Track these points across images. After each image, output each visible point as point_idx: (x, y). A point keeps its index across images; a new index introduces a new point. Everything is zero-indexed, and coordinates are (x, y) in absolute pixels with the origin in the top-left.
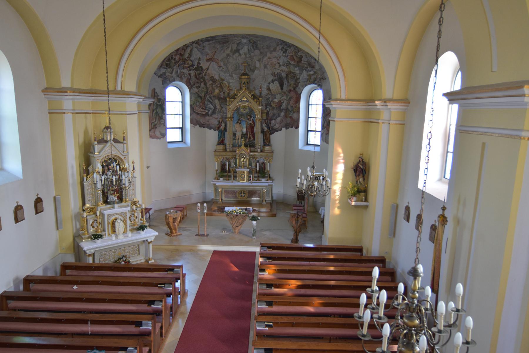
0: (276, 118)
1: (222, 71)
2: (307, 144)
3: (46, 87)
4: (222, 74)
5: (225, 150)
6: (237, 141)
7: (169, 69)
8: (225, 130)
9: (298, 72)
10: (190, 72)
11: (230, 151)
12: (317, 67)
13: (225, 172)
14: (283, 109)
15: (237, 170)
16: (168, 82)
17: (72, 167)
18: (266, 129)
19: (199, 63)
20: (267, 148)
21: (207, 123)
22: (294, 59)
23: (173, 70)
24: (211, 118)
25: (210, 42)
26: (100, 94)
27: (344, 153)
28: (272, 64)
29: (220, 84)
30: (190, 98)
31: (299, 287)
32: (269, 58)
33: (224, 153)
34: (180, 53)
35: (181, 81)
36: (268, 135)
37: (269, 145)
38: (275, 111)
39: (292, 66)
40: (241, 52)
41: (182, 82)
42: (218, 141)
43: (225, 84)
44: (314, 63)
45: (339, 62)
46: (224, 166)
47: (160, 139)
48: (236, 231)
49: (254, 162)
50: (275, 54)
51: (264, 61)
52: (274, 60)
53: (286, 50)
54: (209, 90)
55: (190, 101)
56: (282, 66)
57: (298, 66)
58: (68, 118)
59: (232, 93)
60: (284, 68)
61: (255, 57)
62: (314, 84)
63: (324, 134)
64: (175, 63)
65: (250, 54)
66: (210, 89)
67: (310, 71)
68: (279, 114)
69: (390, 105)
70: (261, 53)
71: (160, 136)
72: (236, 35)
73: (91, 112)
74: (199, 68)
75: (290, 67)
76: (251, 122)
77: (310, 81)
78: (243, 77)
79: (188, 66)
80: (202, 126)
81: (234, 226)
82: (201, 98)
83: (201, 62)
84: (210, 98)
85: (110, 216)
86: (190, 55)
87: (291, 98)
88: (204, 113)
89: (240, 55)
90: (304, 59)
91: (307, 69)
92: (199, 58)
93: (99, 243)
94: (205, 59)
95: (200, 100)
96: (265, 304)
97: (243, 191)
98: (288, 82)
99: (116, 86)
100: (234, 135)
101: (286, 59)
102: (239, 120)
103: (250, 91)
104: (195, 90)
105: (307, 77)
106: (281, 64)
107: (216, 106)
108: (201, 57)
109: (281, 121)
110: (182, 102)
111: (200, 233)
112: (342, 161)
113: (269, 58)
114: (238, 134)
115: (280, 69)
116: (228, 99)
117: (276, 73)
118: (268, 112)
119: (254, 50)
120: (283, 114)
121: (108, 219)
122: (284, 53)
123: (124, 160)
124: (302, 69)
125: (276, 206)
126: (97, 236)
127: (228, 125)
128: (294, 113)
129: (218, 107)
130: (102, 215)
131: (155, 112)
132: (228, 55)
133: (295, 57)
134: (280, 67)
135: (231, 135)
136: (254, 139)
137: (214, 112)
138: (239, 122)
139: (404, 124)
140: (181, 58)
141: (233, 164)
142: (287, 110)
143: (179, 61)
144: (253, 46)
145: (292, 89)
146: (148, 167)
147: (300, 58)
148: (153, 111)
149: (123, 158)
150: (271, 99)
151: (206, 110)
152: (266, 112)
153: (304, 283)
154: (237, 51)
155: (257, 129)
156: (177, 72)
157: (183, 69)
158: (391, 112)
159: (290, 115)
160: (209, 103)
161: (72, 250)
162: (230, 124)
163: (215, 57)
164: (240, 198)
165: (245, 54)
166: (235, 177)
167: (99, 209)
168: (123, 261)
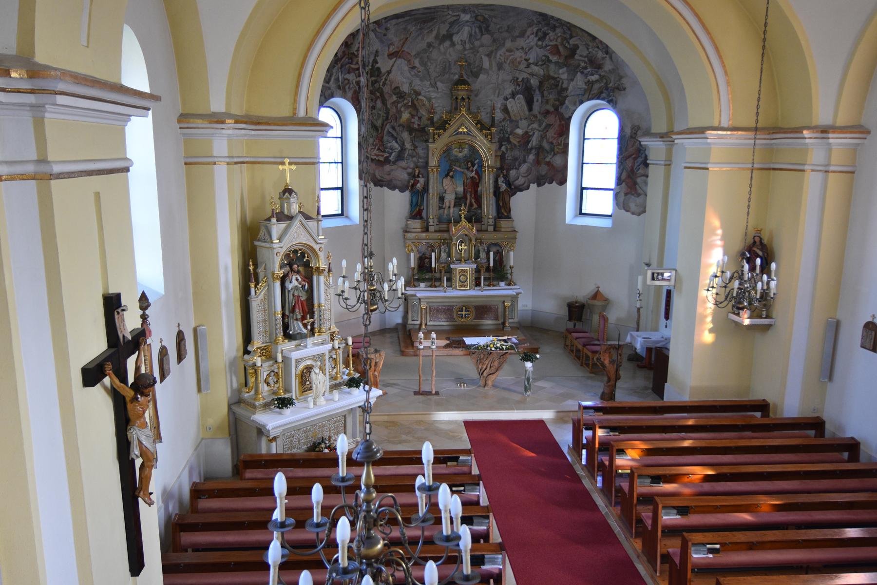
0: (520, 165)
1: (416, 75)
2: (581, 213)
3: (181, 111)
4: (417, 82)
5: (426, 229)
6: (446, 211)
8: (426, 189)
9: (564, 76)
11: (435, 231)
12: (608, 66)
14: (532, 149)
15: (452, 266)
17: (226, 268)
18: (503, 187)
19: (375, 61)
20: (504, 223)
21: (387, 178)
22: (558, 53)
24: (394, 167)
25: (400, 20)
26: (268, 124)
27: (723, 227)
29: (413, 102)
30: (359, 130)
31: (707, 478)
32: (510, 51)
36: (507, 198)
37: (509, 217)
38: (516, 153)
39: (552, 67)
40: (456, 38)
42: (411, 211)
44: (603, 58)
45: (720, 57)
48: (490, 383)
50: (521, 42)
51: (498, 56)
52: (518, 54)
53: (545, 35)
54: (391, 113)
56: (532, 66)
57: (565, 65)
58: (221, 172)
60: (535, 69)
61: (481, 50)
62: (598, 98)
63: (622, 197)
67: (592, 75)
68: (524, 157)
69: (835, 140)
70: (494, 41)
72: (452, 6)
73: (247, 160)
74: (375, 72)
76: (473, 174)
77: (589, 93)
78: (460, 87)
80: (379, 183)
81: (485, 374)
83: (378, 59)
84: (393, 128)
85: (298, 362)
87: (549, 126)
88: (382, 159)
89: (453, 44)
90: (582, 51)
91: (586, 71)
92: (377, 52)
93: (289, 416)
94: (386, 53)
95: (375, 134)
96: (675, 511)
97: (465, 306)
98: (543, 96)
99: (295, 109)
100: (442, 199)
101: (541, 53)
102: (450, 170)
103: (474, 115)
105: (585, 87)
107: (403, 144)
109: (529, 171)
110: (341, 138)
111: (425, 388)
112: (719, 243)
113: (510, 51)
114: (450, 198)
115: (529, 70)
116: (431, 130)
117: (520, 80)
118: (503, 154)
119: (482, 35)
120: (531, 157)
121: (296, 367)
122: (539, 40)
123: (320, 254)
124: (574, 71)
125: (534, 334)
126: (284, 403)
127: (431, 182)
128: (555, 154)
129: (408, 146)
130: (286, 359)
132: (429, 45)
133: (561, 48)
134: (528, 66)
135: (436, 199)
136: (480, 206)
137: (400, 157)
138: (451, 174)
139: (853, 172)
140: (347, 52)
142: (540, 149)
143: (342, 58)
144: (480, 28)
145: (552, 109)
147: (573, 51)
149: (317, 250)
150: (509, 130)
151: (384, 152)
152: (500, 153)
153: (719, 472)
154: (449, 36)
156: (337, 79)
157: (349, 73)
158: (830, 150)
159: (547, 159)
160: (390, 139)
161: (227, 432)
162: (434, 177)
163: (405, 48)
164: (460, 321)
165: (463, 43)
166: (449, 280)
167: (280, 348)
168: (326, 448)
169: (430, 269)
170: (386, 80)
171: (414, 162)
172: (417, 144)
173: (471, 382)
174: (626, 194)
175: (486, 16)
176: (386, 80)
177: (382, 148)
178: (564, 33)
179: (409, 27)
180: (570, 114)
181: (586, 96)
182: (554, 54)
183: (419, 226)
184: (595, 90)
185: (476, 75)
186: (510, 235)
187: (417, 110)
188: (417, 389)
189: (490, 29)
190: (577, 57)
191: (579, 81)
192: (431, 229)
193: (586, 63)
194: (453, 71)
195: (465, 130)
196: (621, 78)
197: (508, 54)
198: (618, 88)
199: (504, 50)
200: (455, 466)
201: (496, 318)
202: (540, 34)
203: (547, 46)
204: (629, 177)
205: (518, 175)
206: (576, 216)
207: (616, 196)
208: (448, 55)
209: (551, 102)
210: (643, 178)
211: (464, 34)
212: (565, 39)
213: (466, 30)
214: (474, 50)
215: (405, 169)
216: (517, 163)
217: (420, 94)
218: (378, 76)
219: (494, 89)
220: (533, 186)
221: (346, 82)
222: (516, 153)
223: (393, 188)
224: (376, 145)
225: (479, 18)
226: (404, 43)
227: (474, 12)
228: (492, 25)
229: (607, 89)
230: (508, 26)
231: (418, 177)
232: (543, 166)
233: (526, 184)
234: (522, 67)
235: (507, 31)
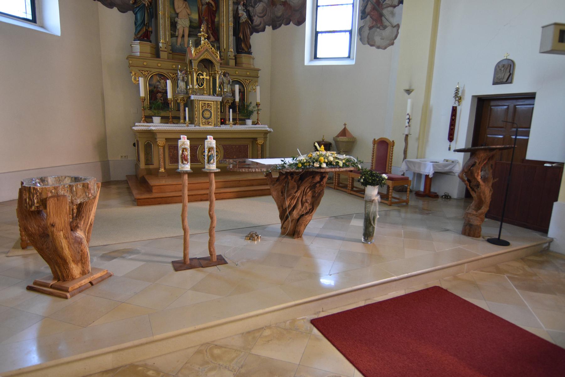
2: (316, 58)
5: (157, 54)
6: (180, 39)
15: (193, 97)
20: (244, 58)
33: (154, 63)
63: (366, 31)
100: (174, 25)
135: (168, 23)
169: (166, 104)
174: (371, 28)
183: (149, 51)
188: (179, 255)
192: (163, 55)
204: (374, 9)
206: (311, 60)
210: (390, 9)
220: (269, 29)
233: (262, 26)
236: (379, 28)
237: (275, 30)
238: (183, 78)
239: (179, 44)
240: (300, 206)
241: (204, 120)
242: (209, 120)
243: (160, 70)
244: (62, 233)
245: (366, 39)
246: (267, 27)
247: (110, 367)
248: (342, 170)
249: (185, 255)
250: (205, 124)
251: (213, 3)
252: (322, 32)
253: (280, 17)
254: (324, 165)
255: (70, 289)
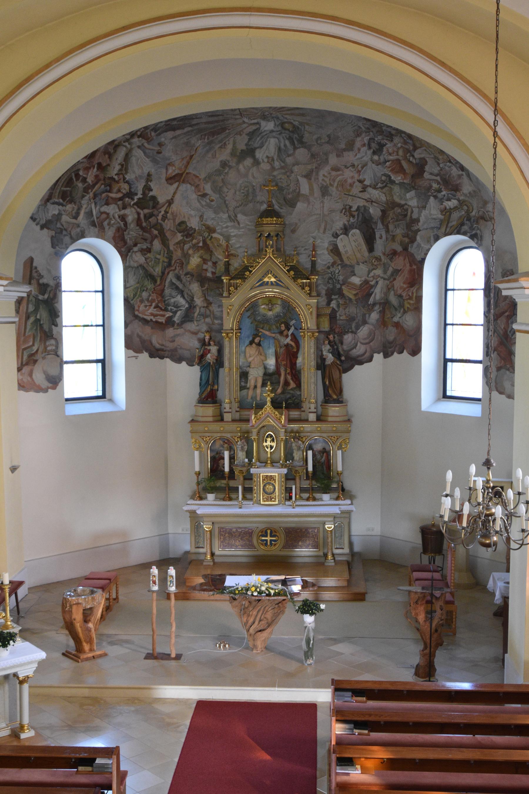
1: (209, 206)
2: (445, 396)
4: (209, 214)
6: (251, 392)
7: (69, 207)
8: (219, 362)
9: (413, 203)
10: (122, 212)
11: (234, 421)
12: (467, 188)
13: (218, 479)
14: (374, 304)
15: (253, 471)
16: (67, 239)
18: (330, 358)
19: (147, 188)
20: (334, 410)
21: (171, 346)
22: (402, 170)
23: (79, 209)
24: (180, 331)
28: (342, 184)
29: (204, 242)
30: (126, 281)
32: (336, 169)
34: (99, 164)
35: (101, 235)
36: (336, 374)
37: (339, 401)
38: (352, 310)
39: (396, 189)
40: (259, 154)
41: (103, 238)
42: (201, 394)
43: (218, 240)
44: (460, 176)
46: (217, 459)
47: (45, 391)
49: (299, 448)
50: (350, 157)
51: (321, 178)
53: (381, 146)
54: (175, 258)
55: (125, 287)
56: (370, 190)
57: (413, 187)
59: (236, 264)
60: (375, 194)
61: (296, 169)
62: (458, 233)
64: (86, 190)
65: (284, 162)
66: (178, 254)
67: (449, 200)
68: (364, 315)
70: (313, 156)
71: (45, 384)
72: (246, 110)
74: (148, 202)
75: (391, 189)
76: (288, 340)
79: (119, 195)
80: (156, 353)
81: (252, 631)
82: (153, 278)
83: (152, 184)
84: (178, 278)
86: (125, 167)
87: (396, 272)
88: (162, 320)
89: (257, 163)
90: (431, 168)
91: (440, 195)
92: (149, 175)
94: (164, 176)
95: (150, 286)
97: (270, 530)
98: (387, 231)
100: (244, 375)
101: (380, 170)
102: (256, 336)
104: (139, 258)
105: (441, 217)
106: (367, 183)
107: (192, 300)
108: (153, 171)
109: (371, 336)
110: (103, 292)
111: (159, 650)
114: (256, 375)
115: (366, 196)
116: (225, 279)
117: (354, 208)
118: (334, 312)
119: (295, 148)
120: (374, 316)
122: (374, 153)
124: (425, 194)
127: (226, 351)
128: (405, 312)
129: (199, 301)
131: (32, 319)
132: (224, 164)
133: (405, 164)
135: (236, 376)
136: (299, 386)
137: (188, 317)
138: (257, 340)
140: (101, 176)
141: (241, 456)
142: (385, 304)
144: (291, 139)
145: (399, 249)
146: (13, 469)
147: (421, 167)
148: (28, 318)
150: (341, 278)
151: (166, 310)
152: (328, 311)
154: (250, 152)
155: (306, 359)
156: (90, 214)
157: (107, 204)
159: (396, 319)
160: (174, 293)
162: (231, 348)
163: (190, 170)
164: (262, 550)
165: (270, 160)
166: (248, 491)
170: (166, 212)
171: (207, 324)
172: (211, 299)
173: (238, 642)
174: (499, 369)
175: (296, 123)
176: (166, 212)
177: (163, 305)
178: (405, 143)
179: (193, 140)
180: (422, 256)
181: (443, 230)
182: (397, 172)
184: (454, 223)
185: (292, 204)
186: (342, 427)
187: (211, 253)
189: (305, 140)
190: (426, 175)
191: (433, 210)
192: (227, 417)
193: (438, 183)
194: (259, 198)
195: (273, 280)
196: (485, 203)
197: (334, 173)
198: (483, 218)
199: (327, 168)
200: (89, 773)
201: (316, 546)
202: (374, 146)
203: (386, 161)
205: (356, 341)
206: (438, 400)
207: (486, 371)
208: (250, 177)
209: (399, 238)
211: (270, 148)
212: (408, 151)
213: (272, 144)
214: (287, 170)
215: (195, 333)
216: (353, 325)
217: (214, 231)
218: (154, 207)
219: (318, 224)
220: (378, 357)
221: (104, 216)
222: (352, 310)
223: (178, 360)
224: (153, 301)
225: (287, 125)
226: (188, 163)
227: (278, 118)
228: (306, 135)
229: (469, 219)
230: (329, 136)
231: (209, 345)
232: (390, 328)
233: (367, 354)
234: (356, 189)
235: (328, 142)
236: (508, 370)
237: (387, 359)
238: (242, 447)
239: (249, 398)
240: (257, 623)
241: (266, 496)
242: (273, 496)
243: (223, 435)
244: (78, 624)
245: (493, 384)
246: (376, 355)
247: (87, 695)
248: (273, 598)
249: (153, 649)
250: (267, 500)
251: (293, 344)
252: (452, 361)
253: (390, 343)
254: (255, 594)
255: (81, 658)
